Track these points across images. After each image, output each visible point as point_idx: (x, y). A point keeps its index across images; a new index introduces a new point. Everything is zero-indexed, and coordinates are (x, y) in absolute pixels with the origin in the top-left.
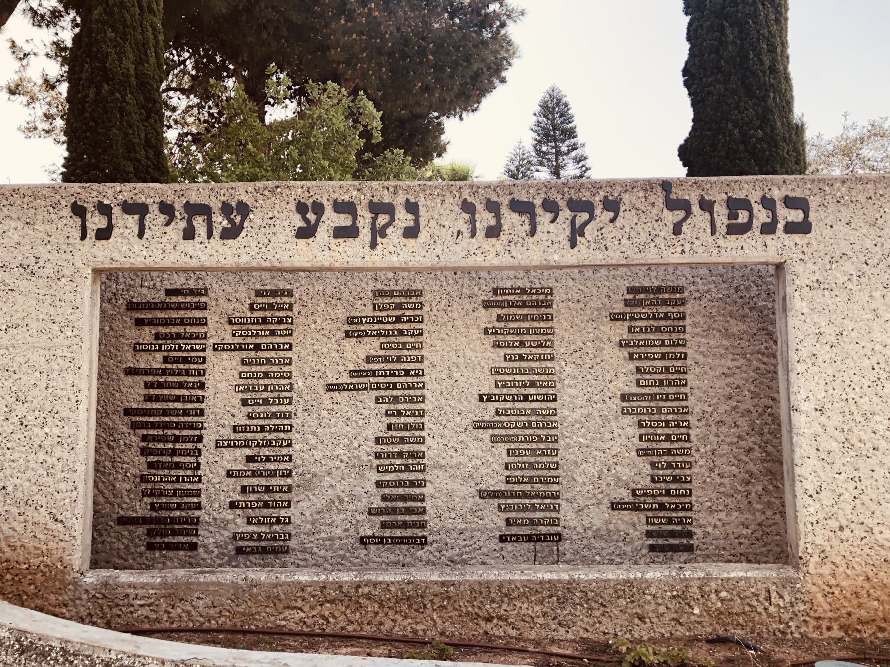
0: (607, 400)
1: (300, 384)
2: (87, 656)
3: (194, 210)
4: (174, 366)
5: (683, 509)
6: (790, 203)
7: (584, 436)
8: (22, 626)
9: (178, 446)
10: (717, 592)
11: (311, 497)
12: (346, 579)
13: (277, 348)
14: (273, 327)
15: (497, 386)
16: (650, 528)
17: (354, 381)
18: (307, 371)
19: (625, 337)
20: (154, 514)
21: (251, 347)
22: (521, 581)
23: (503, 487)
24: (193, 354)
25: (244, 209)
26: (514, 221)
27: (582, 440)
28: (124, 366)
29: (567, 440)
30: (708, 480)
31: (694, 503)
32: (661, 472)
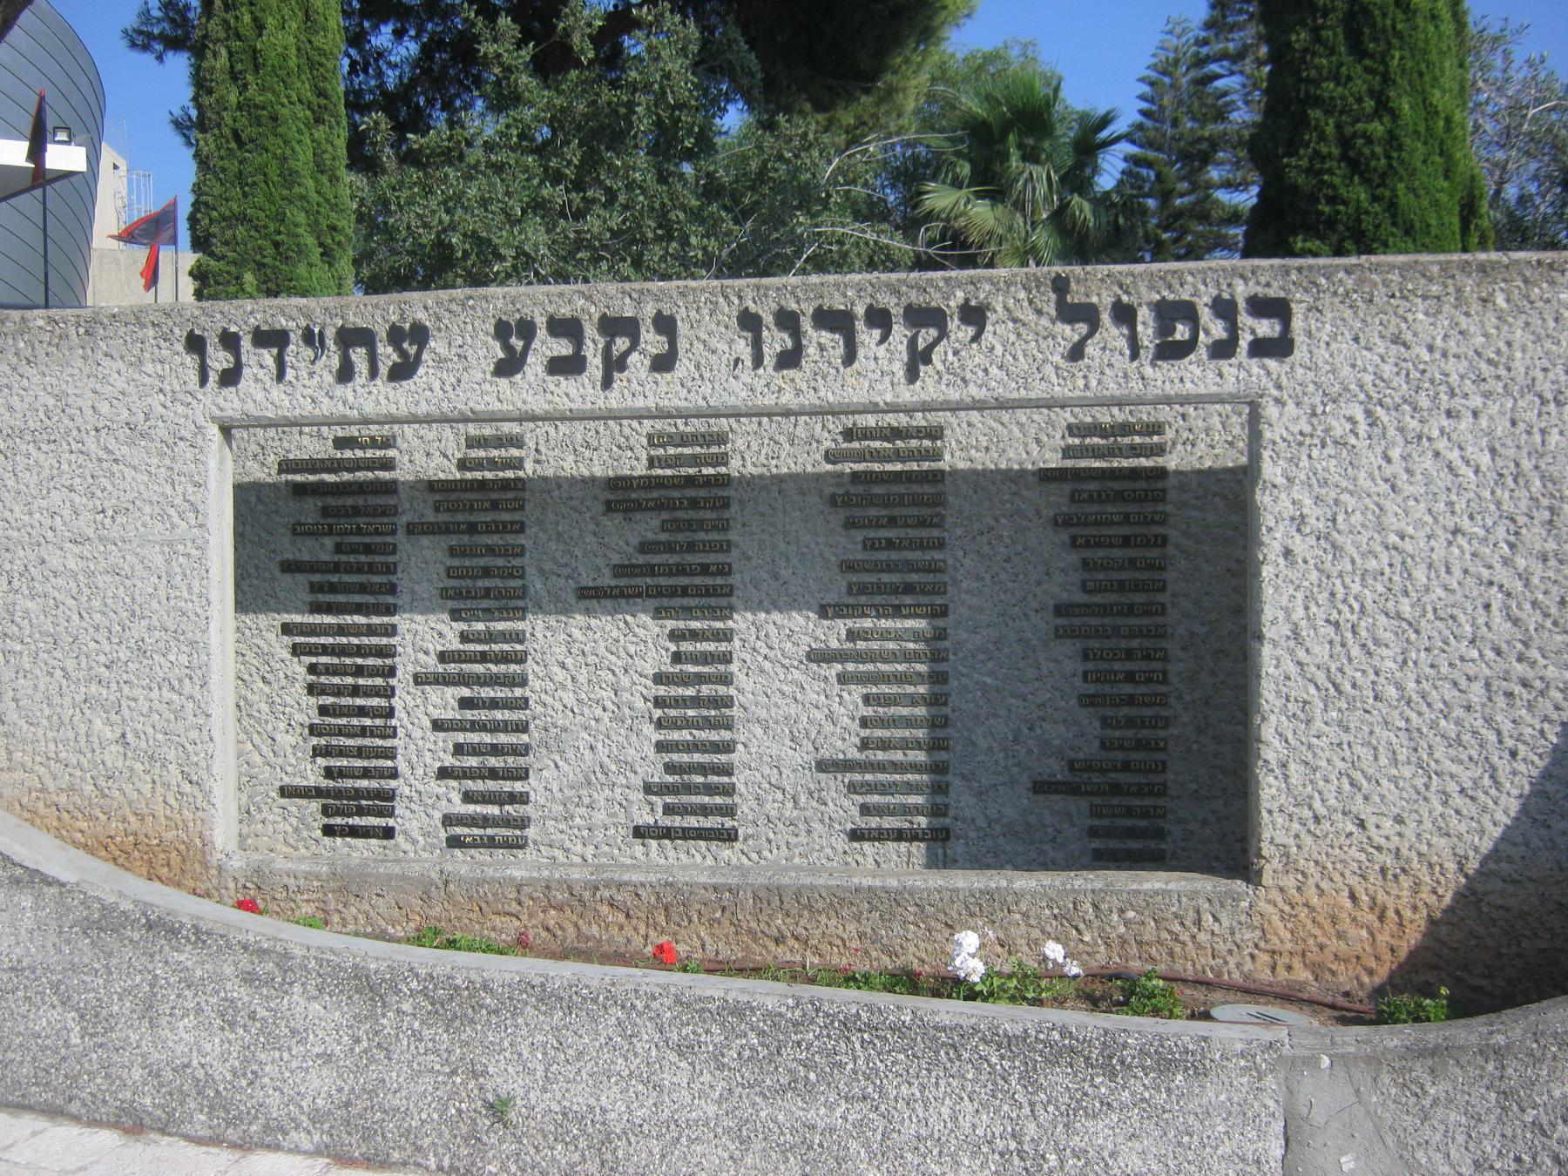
0: (1032, 614)
1: (538, 586)
2: (222, 936)
3: (351, 337)
4: (352, 559)
5: (1151, 793)
6: (1260, 307)
7: (991, 674)
8: (148, 898)
9: (361, 681)
10: (1122, 911)
11: (560, 763)
12: (577, 876)
13: (502, 528)
14: (494, 496)
15: (850, 592)
16: (1096, 822)
17: (623, 582)
18: (548, 566)
19: (1064, 509)
20: (331, 783)
21: (463, 527)
22: (827, 887)
23: (853, 754)
24: (378, 539)
25: (420, 334)
26: (822, 340)
27: (988, 680)
28: (279, 558)
29: (964, 681)
30: (1195, 747)
31: (1170, 784)
32: (1117, 733)
